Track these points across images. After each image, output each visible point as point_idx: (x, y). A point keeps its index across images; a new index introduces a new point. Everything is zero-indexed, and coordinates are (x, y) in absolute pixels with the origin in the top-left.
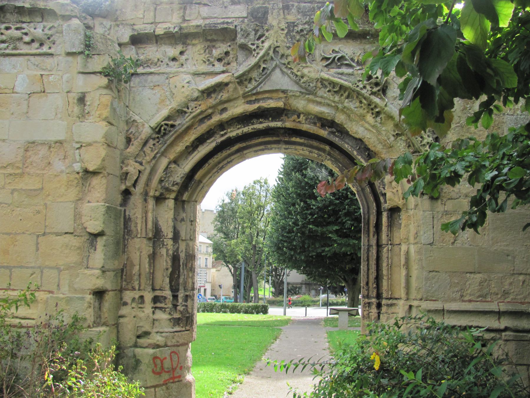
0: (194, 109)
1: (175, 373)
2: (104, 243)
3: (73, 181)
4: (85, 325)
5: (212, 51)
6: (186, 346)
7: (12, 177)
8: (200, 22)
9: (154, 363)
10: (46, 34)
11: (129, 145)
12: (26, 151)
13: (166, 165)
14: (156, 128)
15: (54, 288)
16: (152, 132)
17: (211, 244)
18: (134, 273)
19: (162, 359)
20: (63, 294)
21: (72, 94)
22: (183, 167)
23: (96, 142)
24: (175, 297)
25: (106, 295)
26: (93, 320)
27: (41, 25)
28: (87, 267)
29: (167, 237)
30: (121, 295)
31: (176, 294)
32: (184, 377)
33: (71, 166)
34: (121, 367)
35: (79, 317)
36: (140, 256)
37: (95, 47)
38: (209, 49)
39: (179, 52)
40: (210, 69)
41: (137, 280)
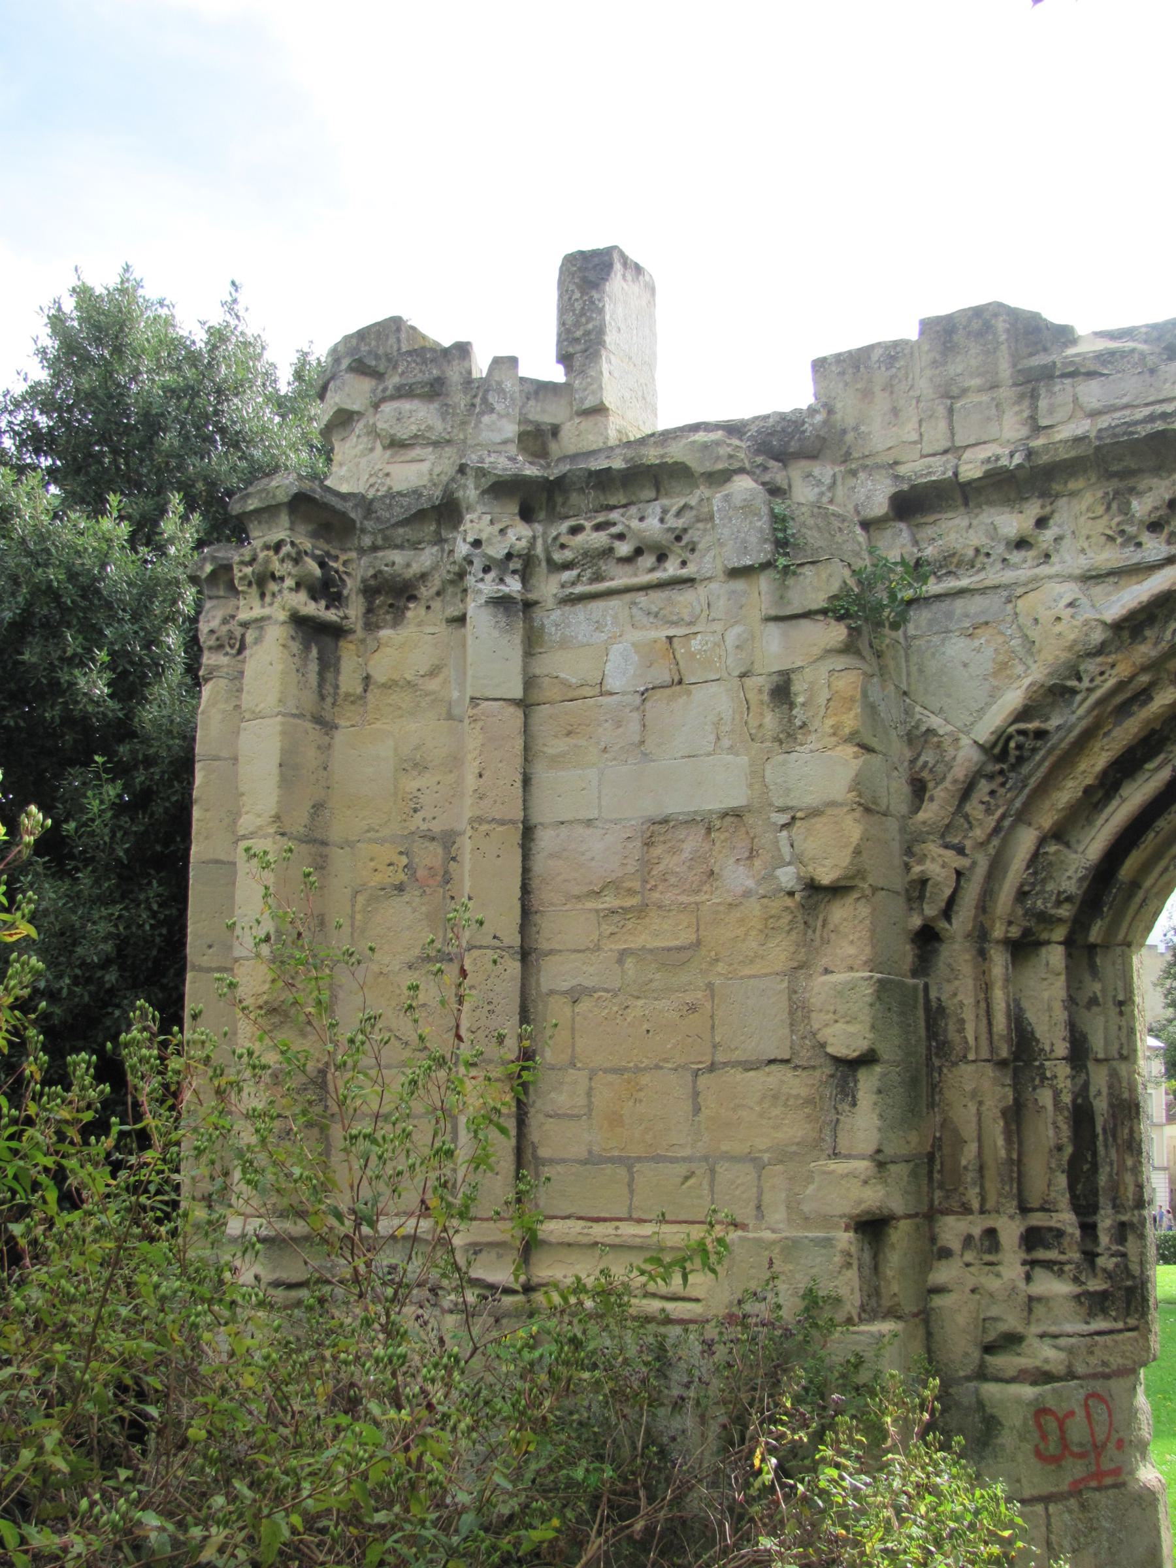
0: (1099, 679)
1: (1102, 1458)
2: (877, 1084)
3: (779, 918)
4: (840, 1317)
5: (1129, 503)
6: (1132, 1377)
7: (616, 918)
8: (1082, 427)
9: (1039, 1426)
10: (670, 530)
11: (922, 801)
12: (646, 844)
13: (1033, 848)
14: (995, 744)
15: (745, 1213)
16: (983, 758)
17: (1157, 1049)
18: (964, 1162)
19: (1061, 1415)
20: (774, 1231)
21: (754, 679)
22: (1080, 849)
23: (832, 804)
24: (1089, 1230)
25: (891, 1231)
26: (858, 1303)
27: (655, 509)
28: (835, 1154)
29: (1054, 1055)
30: (931, 1228)
31: (1090, 1220)
32: (1132, 1472)
33: (770, 876)
34: (960, 1438)
35: (821, 1294)
36: (979, 1114)
37: (801, 541)
38: (1119, 500)
39: (1032, 522)
40: (1129, 556)
41: (975, 1184)
